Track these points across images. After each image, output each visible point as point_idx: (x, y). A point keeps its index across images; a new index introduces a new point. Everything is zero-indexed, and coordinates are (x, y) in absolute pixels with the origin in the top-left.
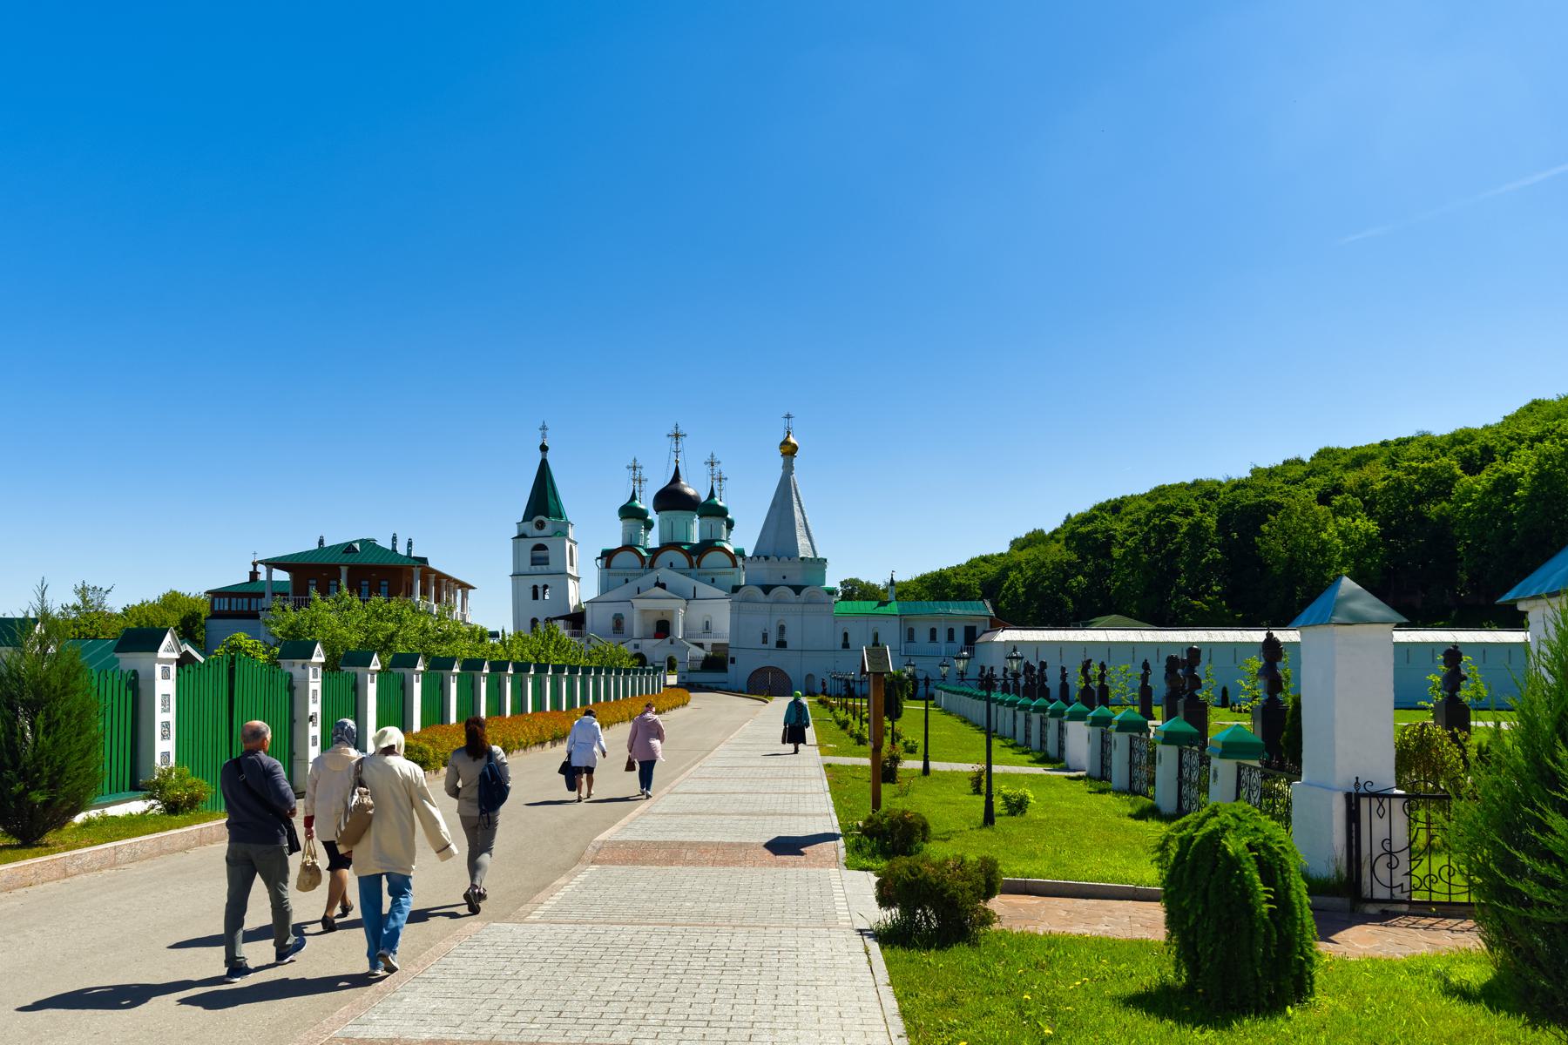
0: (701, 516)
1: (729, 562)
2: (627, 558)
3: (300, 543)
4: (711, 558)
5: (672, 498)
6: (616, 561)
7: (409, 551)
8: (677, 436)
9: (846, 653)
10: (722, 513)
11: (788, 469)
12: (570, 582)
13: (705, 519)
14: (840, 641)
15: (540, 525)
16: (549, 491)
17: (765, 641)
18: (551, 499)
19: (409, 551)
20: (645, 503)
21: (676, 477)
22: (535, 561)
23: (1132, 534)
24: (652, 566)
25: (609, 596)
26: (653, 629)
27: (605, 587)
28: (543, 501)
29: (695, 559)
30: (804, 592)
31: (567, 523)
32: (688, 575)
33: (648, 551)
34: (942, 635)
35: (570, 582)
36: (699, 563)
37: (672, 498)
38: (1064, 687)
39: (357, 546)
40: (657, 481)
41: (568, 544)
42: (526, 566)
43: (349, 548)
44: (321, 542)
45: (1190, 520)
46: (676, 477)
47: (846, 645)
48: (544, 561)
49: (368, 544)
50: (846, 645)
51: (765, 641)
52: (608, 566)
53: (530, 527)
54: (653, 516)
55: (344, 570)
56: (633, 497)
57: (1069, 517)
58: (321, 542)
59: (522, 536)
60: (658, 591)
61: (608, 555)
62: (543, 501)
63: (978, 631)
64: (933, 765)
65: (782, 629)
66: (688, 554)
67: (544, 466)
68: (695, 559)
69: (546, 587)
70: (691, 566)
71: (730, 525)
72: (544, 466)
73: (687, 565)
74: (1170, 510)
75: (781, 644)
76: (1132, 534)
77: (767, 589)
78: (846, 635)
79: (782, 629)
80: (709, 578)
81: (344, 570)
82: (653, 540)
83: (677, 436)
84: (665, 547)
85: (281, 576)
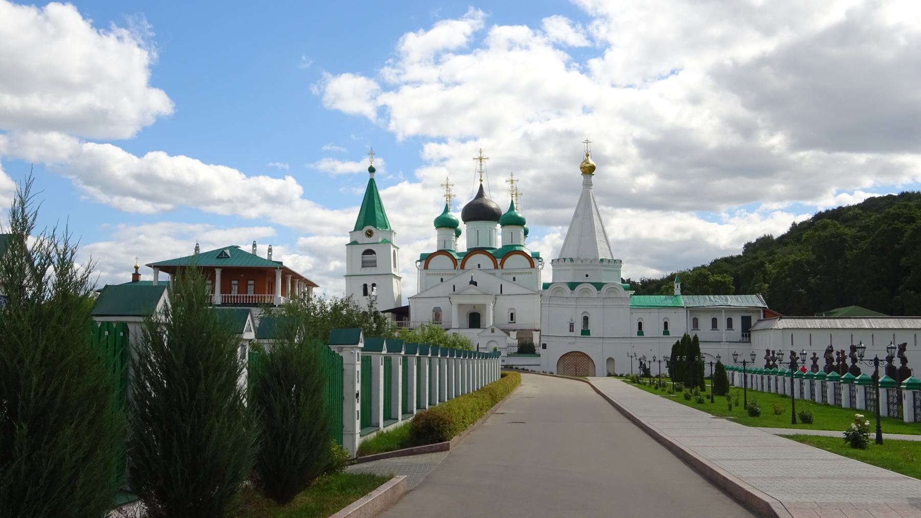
0: (503, 225)
1: (529, 265)
2: (443, 262)
3: (181, 250)
4: (512, 262)
5: (478, 211)
6: (433, 263)
7: (270, 256)
8: (481, 159)
9: (640, 341)
10: (520, 222)
11: (588, 185)
12: (394, 280)
13: (507, 228)
14: (662, 329)
15: (370, 234)
16: (377, 205)
17: (572, 330)
18: (378, 213)
19: (270, 256)
20: (456, 215)
21: (481, 193)
22: (365, 264)
23: (862, 238)
24: (462, 267)
25: (427, 294)
26: (466, 321)
27: (424, 287)
28: (371, 214)
29: (499, 261)
30: (604, 289)
31: (391, 231)
32: (494, 274)
33: (458, 254)
34: (722, 323)
35: (394, 280)
36: (502, 264)
37: (478, 211)
38: (815, 367)
39: (228, 252)
40: (464, 198)
41: (392, 249)
42: (358, 268)
43: (221, 254)
44: (197, 249)
45: (913, 226)
46: (481, 193)
47: (640, 332)
48: (373, 264)
49: (234, 249)
50: (640, 332)
51: (572, 330)
52: (426, 267)
53: (361, 236)
54: (462, 226)
55: (218, 273)
56: (447, 210)
57: (794, 224)
58: (197, 249)
59: (354, 243)
60: (473, 289)
61: (426, 259)
62: (371, 214)
63: (753, 321)
64: (885, 436)
65: (586, 319)
66: (493, 257)
67: (372, 182)
68: (499, 261)
69: (374, 285)
70: (496, 267)
71: (526, 233)
72: (372, 182)
73: (492, 266)
74: (896, 217)
75: (586, 332)
76: (862, 238)
77: (573, 286)
78: (640, 324)
79: (586, 319)
80: (511, 278)
81: (218, 273)
82: (461, 245)
83: (481, 159)
84: (472, 251)
85: (164, 277)
